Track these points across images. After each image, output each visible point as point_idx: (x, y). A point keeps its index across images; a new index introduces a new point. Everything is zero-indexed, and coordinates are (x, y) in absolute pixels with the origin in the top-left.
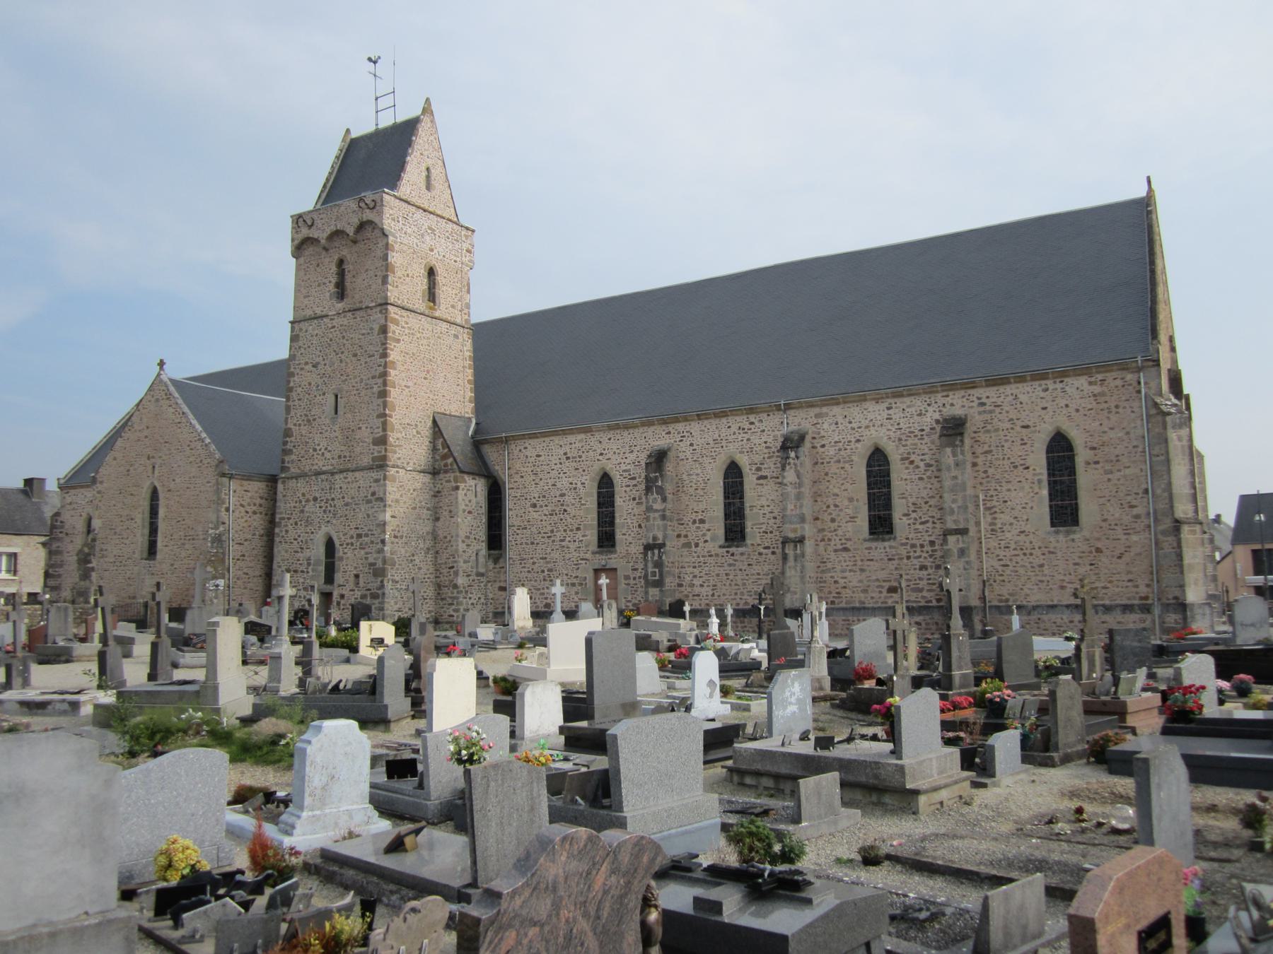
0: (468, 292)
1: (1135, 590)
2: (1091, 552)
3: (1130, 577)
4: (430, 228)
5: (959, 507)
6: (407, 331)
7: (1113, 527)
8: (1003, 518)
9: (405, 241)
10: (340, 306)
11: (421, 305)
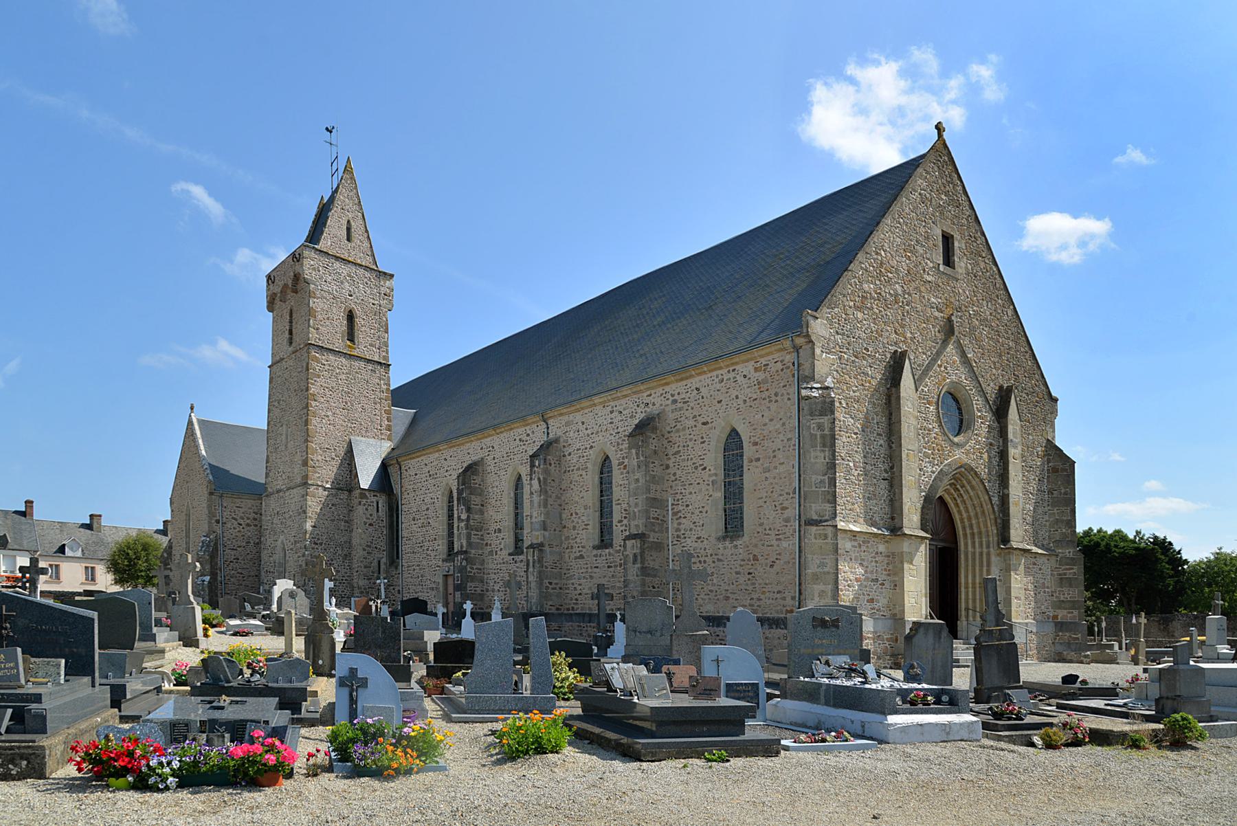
0: (387, 332)
1: (782, 602)
2: (749, 560)
3: (780, 588)
4: (349, 276)
5: (639, 511)
6: (327, 367)
7: (767, 532)
8: (686, 523)
9: (325, 288)
10: (291, 349)
11: (339, 343)
